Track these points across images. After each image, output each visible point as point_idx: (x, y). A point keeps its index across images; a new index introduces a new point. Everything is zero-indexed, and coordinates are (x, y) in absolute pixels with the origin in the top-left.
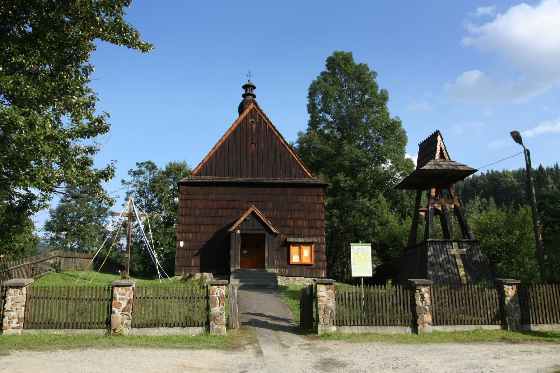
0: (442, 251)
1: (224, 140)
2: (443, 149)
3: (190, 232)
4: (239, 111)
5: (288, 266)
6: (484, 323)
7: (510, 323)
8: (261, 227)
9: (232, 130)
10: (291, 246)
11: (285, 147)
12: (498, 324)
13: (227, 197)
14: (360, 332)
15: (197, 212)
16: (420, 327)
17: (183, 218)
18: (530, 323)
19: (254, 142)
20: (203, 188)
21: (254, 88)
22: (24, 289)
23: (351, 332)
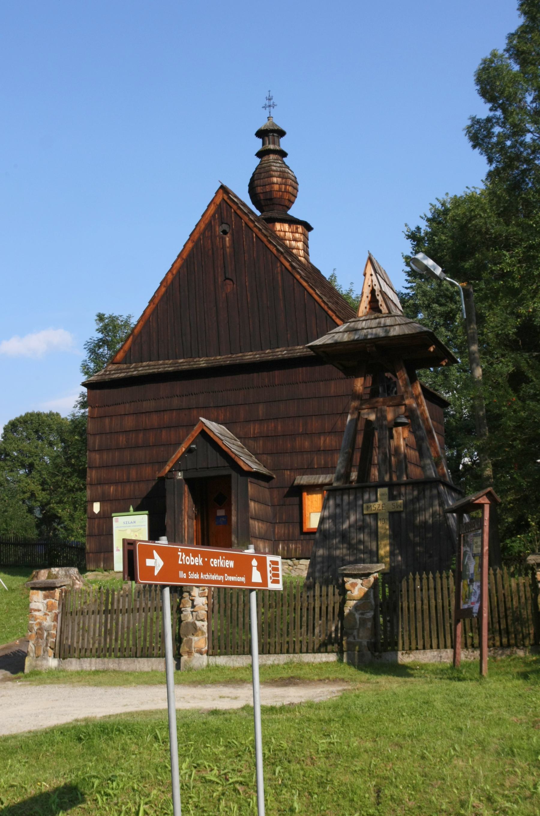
0: (352, 506)
1: (169, 281)
2: (377, 293)
4: (249, 192)
5: (302, 537)
6: (304, 649)
7: (348, 650)
8: (221, 462)
9: (184, 256)
10: (305, 494)
11: (294, 277)
12: (333, 652)
13: (176, 402)
14: (93, 669)
15: (122, 439)
16: (184, 658)
19: (229, 275)
20: (130, 388)
21: (282, 133)
22: (58, 591)
23: (79, 669)
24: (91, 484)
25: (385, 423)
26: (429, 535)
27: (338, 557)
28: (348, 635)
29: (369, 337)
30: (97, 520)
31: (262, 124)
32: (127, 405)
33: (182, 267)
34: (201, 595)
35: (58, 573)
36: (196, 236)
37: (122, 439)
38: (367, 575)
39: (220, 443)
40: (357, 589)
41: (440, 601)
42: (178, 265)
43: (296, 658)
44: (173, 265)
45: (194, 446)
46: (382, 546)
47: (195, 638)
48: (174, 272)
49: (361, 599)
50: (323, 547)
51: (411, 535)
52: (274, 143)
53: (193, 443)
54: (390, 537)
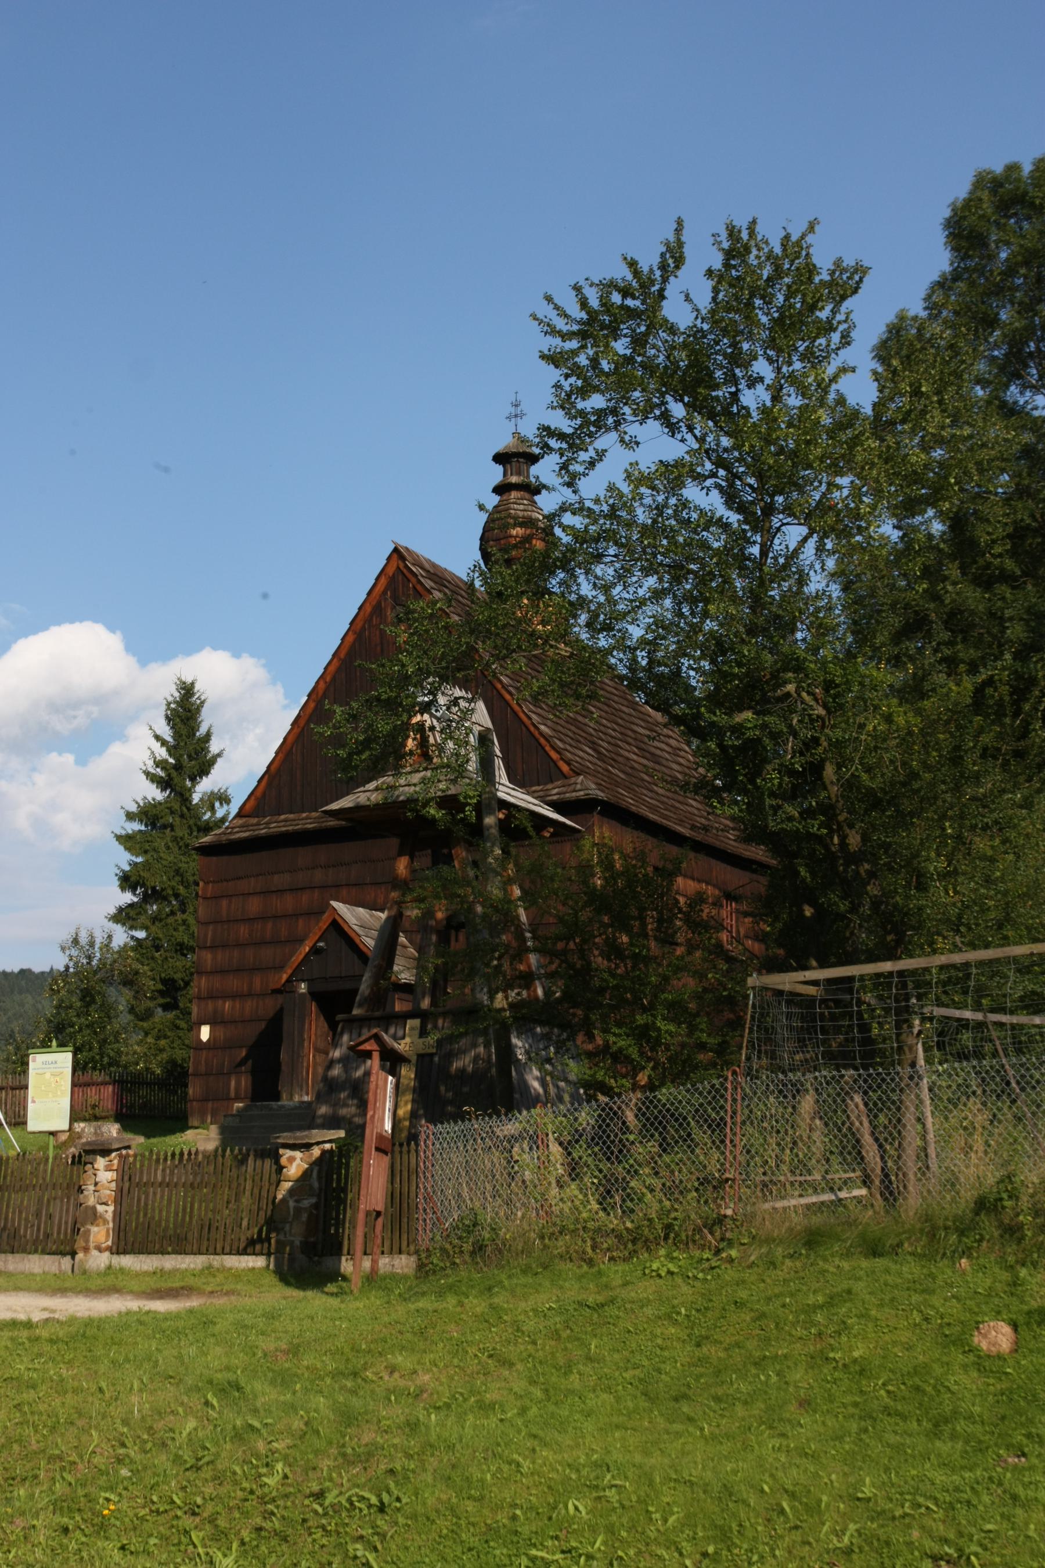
3: (225, 997)
6: (227, 1250)
9: (342, 656)
13: (319, 876)
15: (243, 931)
17: (209, 956)
18: (339, 1253)
24: (199, 998)
25: (433, 923)
26: (466, 1089)
27: (344, 1118)
28: (278, 1230)
29: (401, 798)
30: (204, 1052)
31: (503, 442)
32: (253, 880)
33: (338, 670)
34: (108, 1169)
35: (83, 1130)
36: (359, 624)
37: (243, 931)
38: (308, 1146)
39: (357, 941)
40: (295, 1164)
41: (397, 1185)
42: (332, 668)
43: (216, 1261)
44: (326, 669)
45: (321, 944)
46: (402, 1103)
47: (94, 1229)
48: (328, 679)
49: (297, 1181)
50: (326, 1102)
51: (442, 1089)
52: (519, 474)
53: (318, 941)
54: (414, 1090)
